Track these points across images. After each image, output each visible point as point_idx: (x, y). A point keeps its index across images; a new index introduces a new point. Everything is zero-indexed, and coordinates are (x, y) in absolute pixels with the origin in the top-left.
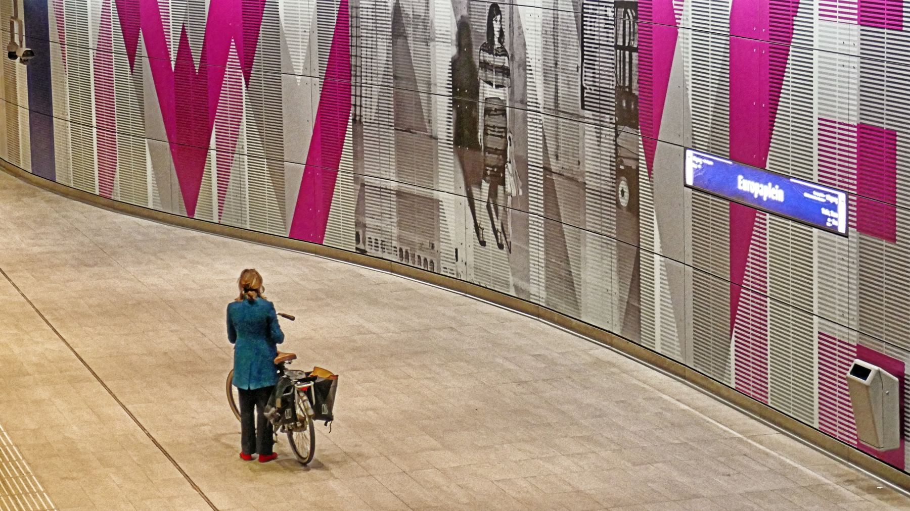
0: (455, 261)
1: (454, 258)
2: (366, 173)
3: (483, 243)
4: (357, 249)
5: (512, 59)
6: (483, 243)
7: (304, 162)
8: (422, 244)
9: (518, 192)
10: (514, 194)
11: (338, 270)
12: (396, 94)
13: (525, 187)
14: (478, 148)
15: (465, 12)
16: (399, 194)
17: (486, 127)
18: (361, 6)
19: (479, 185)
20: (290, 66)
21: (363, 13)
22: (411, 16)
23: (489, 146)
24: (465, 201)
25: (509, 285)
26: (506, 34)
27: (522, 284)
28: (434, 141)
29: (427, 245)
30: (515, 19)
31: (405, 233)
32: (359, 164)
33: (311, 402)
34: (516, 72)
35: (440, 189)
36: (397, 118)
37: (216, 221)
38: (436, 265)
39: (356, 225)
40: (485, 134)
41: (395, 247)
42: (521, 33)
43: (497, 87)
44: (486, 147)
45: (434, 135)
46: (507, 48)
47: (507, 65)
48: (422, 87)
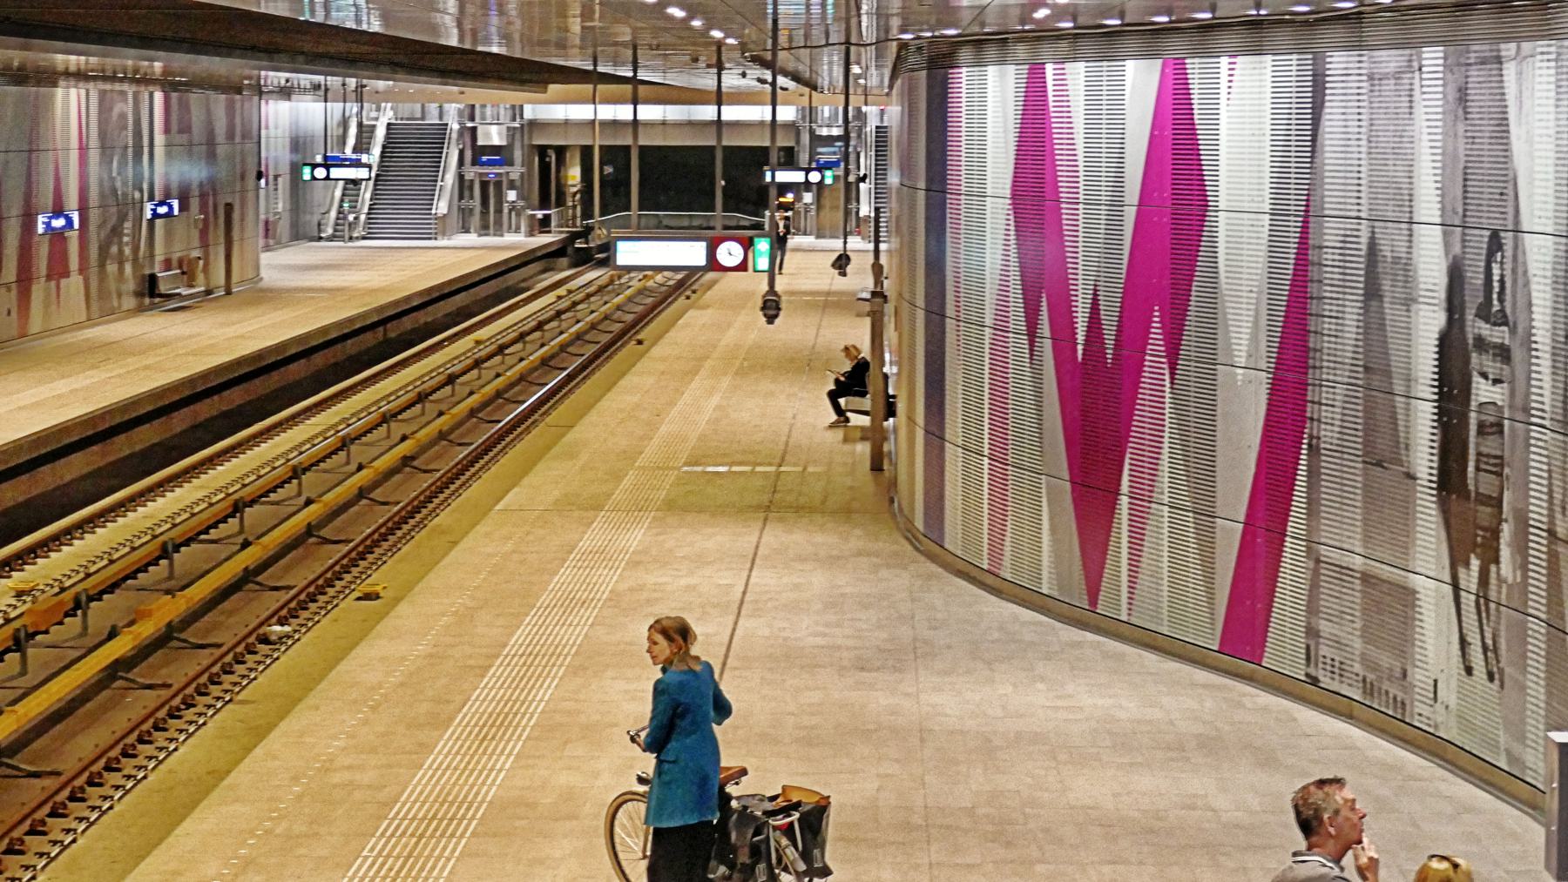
0: (1432, 702)
1: (1432, 696)
2: (1323, 540)
3: (1469, 671)
4: (1307, 675)
5: (1513, 331)
6: (1469, 671)
7: (1242, 518)
8: (1391, 670)
9: (1515, 577)
10: (1510, 580)
11: (1265, 709)
12: (1367, 399)
13: (1524, 567)
14: (1468, 498)
15: (1457, 249)
16: (1366, 578)
17: (1479, 454)
18: (1326, 244)
19: (1467, 564)
20: (1229, 351)
21: (1329, 256)
22: (1389, 260)
23: (1481, 491)
24: (1448, 589)
25: (1498, 748)
26: (1508, 285)
27: (1517, 748)
28: (1410, 482)
29: (1398, 674)
30: (1520, 259)
31: (1374, 653)
32: (1313, 524)
33: (797, 849)
34: (1517, 354)
35: (1418, 570)
36: (1366, 443)
37: (1124, 618)
38: (1408, 707)
39: (1306, 633)
40: (1478, 469)
41: (1357, 675)
42: (1527, 284)
43: (1496, 381)
44: (1477, 493)
45: (1412, 472)
46: (1508, 311)
47: (1507, 342)
48: (1399, 388)
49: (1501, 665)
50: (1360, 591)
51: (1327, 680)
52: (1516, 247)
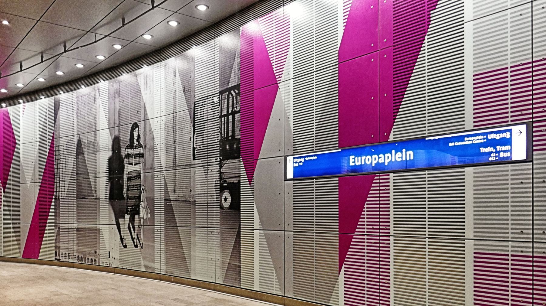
1: (108, 256)
4: (55, 259)
9: (148, 216)
13: (152, 212)
19: (124, 217)
28: (97, 200)
31: (82, 249)
49: (80, 48)
50: (76, 234)
51: (64, 259)
52: (145, 127)
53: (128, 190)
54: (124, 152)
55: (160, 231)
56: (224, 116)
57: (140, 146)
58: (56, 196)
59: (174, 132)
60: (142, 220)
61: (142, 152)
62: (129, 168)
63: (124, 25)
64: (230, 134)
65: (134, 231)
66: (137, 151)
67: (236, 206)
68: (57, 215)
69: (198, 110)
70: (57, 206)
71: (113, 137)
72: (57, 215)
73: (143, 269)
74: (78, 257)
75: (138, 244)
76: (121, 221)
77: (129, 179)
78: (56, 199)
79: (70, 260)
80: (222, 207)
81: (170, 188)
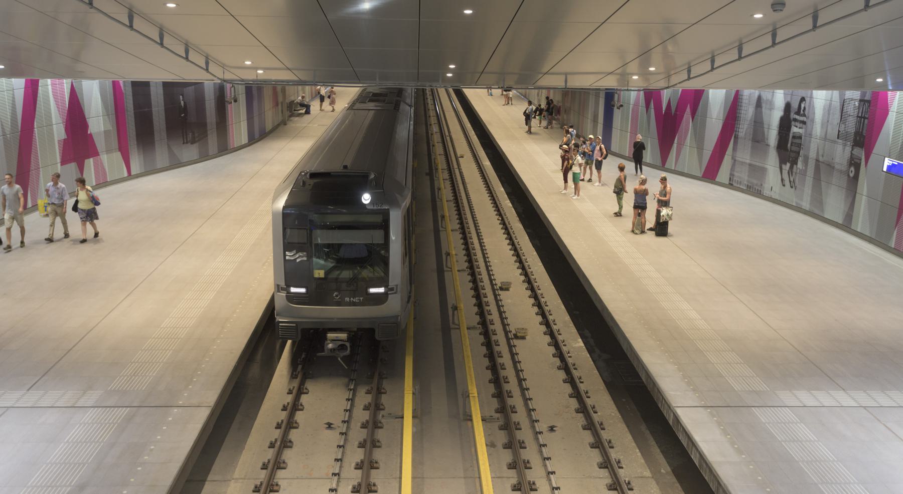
53: (791, 145)
54: (793, 116)
55: (809, 181)
56: (859, 117)
57: (804, 115)
58: (735, 135)
59: (829, 114)
60: (798, 170)
61: (805, 120)
62: (795, 130)
63: (713, 69)
64: (861, 130)
65: (792, 175)
66: (802, 118)
67: (856, 177)
68: (734, 149)
69: (846, 105)
70: (735, 143)
71: (786, 101)
72: (734, 149)
73: (794, 204)
74: (748, 185)
75: (794, 186)
76: (784, 166)
77: (794, 137)
78: (735, 137)
79: (741, 187)
80: (849, 176)
81: (820, 153)
